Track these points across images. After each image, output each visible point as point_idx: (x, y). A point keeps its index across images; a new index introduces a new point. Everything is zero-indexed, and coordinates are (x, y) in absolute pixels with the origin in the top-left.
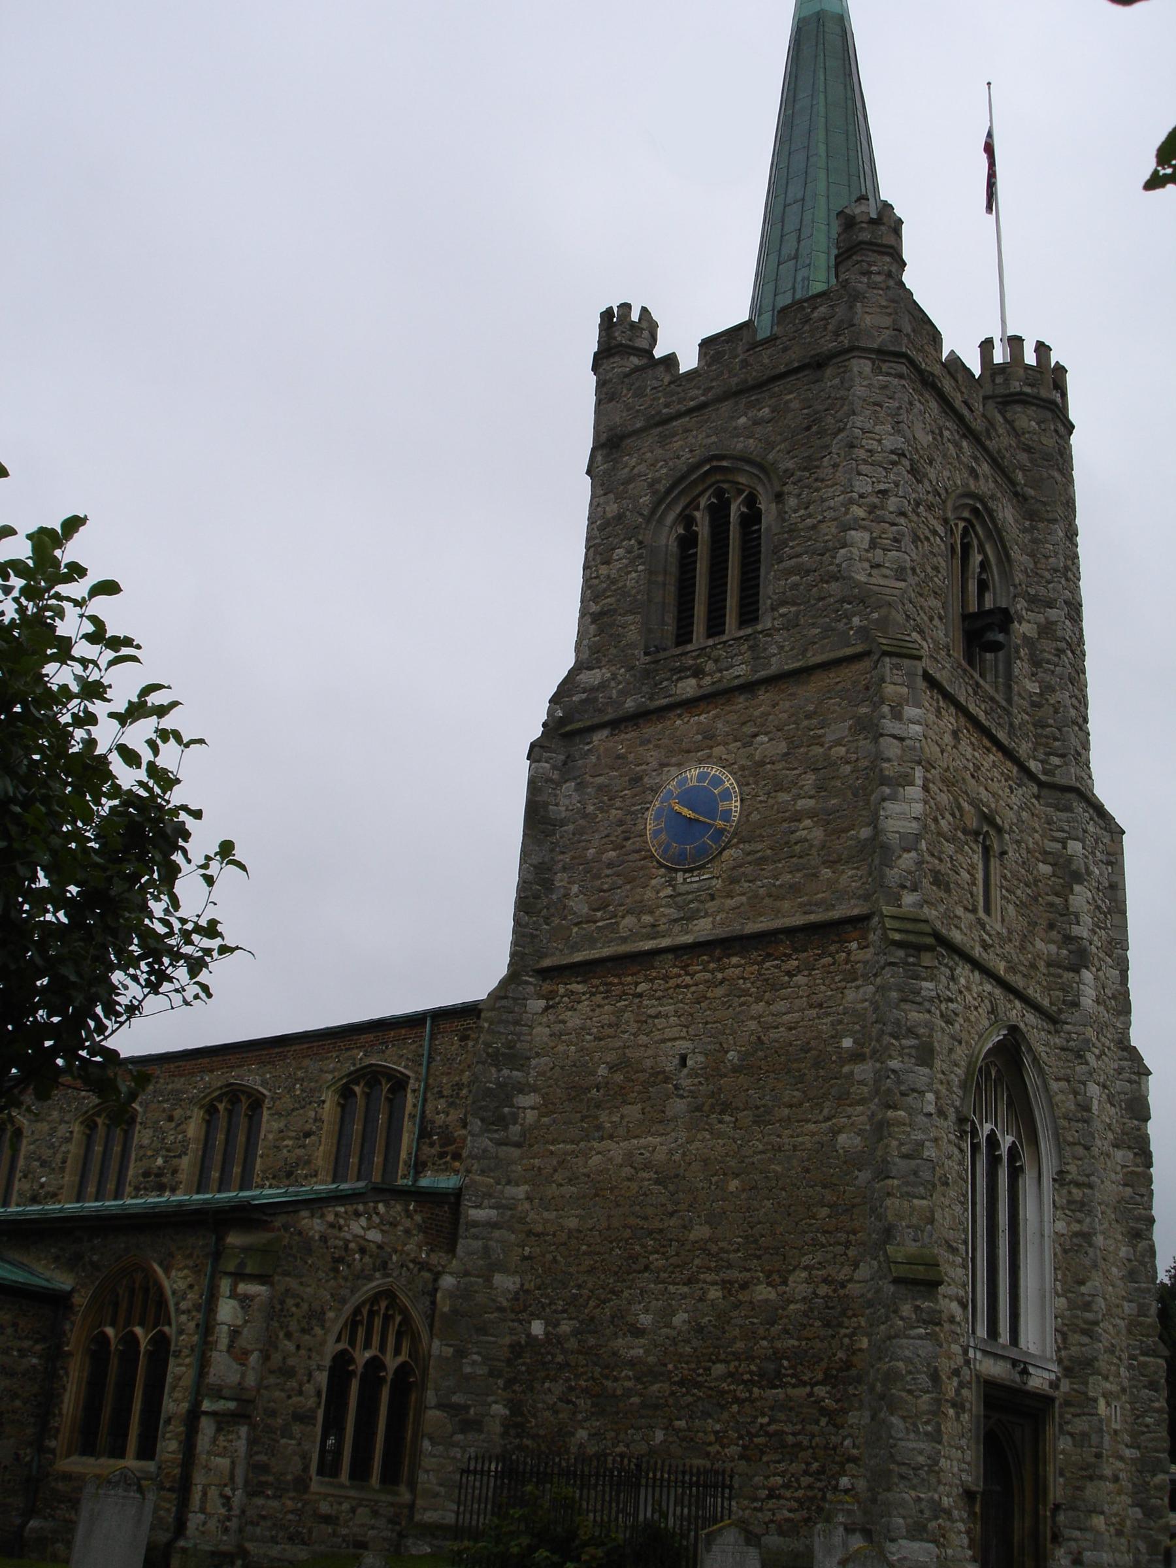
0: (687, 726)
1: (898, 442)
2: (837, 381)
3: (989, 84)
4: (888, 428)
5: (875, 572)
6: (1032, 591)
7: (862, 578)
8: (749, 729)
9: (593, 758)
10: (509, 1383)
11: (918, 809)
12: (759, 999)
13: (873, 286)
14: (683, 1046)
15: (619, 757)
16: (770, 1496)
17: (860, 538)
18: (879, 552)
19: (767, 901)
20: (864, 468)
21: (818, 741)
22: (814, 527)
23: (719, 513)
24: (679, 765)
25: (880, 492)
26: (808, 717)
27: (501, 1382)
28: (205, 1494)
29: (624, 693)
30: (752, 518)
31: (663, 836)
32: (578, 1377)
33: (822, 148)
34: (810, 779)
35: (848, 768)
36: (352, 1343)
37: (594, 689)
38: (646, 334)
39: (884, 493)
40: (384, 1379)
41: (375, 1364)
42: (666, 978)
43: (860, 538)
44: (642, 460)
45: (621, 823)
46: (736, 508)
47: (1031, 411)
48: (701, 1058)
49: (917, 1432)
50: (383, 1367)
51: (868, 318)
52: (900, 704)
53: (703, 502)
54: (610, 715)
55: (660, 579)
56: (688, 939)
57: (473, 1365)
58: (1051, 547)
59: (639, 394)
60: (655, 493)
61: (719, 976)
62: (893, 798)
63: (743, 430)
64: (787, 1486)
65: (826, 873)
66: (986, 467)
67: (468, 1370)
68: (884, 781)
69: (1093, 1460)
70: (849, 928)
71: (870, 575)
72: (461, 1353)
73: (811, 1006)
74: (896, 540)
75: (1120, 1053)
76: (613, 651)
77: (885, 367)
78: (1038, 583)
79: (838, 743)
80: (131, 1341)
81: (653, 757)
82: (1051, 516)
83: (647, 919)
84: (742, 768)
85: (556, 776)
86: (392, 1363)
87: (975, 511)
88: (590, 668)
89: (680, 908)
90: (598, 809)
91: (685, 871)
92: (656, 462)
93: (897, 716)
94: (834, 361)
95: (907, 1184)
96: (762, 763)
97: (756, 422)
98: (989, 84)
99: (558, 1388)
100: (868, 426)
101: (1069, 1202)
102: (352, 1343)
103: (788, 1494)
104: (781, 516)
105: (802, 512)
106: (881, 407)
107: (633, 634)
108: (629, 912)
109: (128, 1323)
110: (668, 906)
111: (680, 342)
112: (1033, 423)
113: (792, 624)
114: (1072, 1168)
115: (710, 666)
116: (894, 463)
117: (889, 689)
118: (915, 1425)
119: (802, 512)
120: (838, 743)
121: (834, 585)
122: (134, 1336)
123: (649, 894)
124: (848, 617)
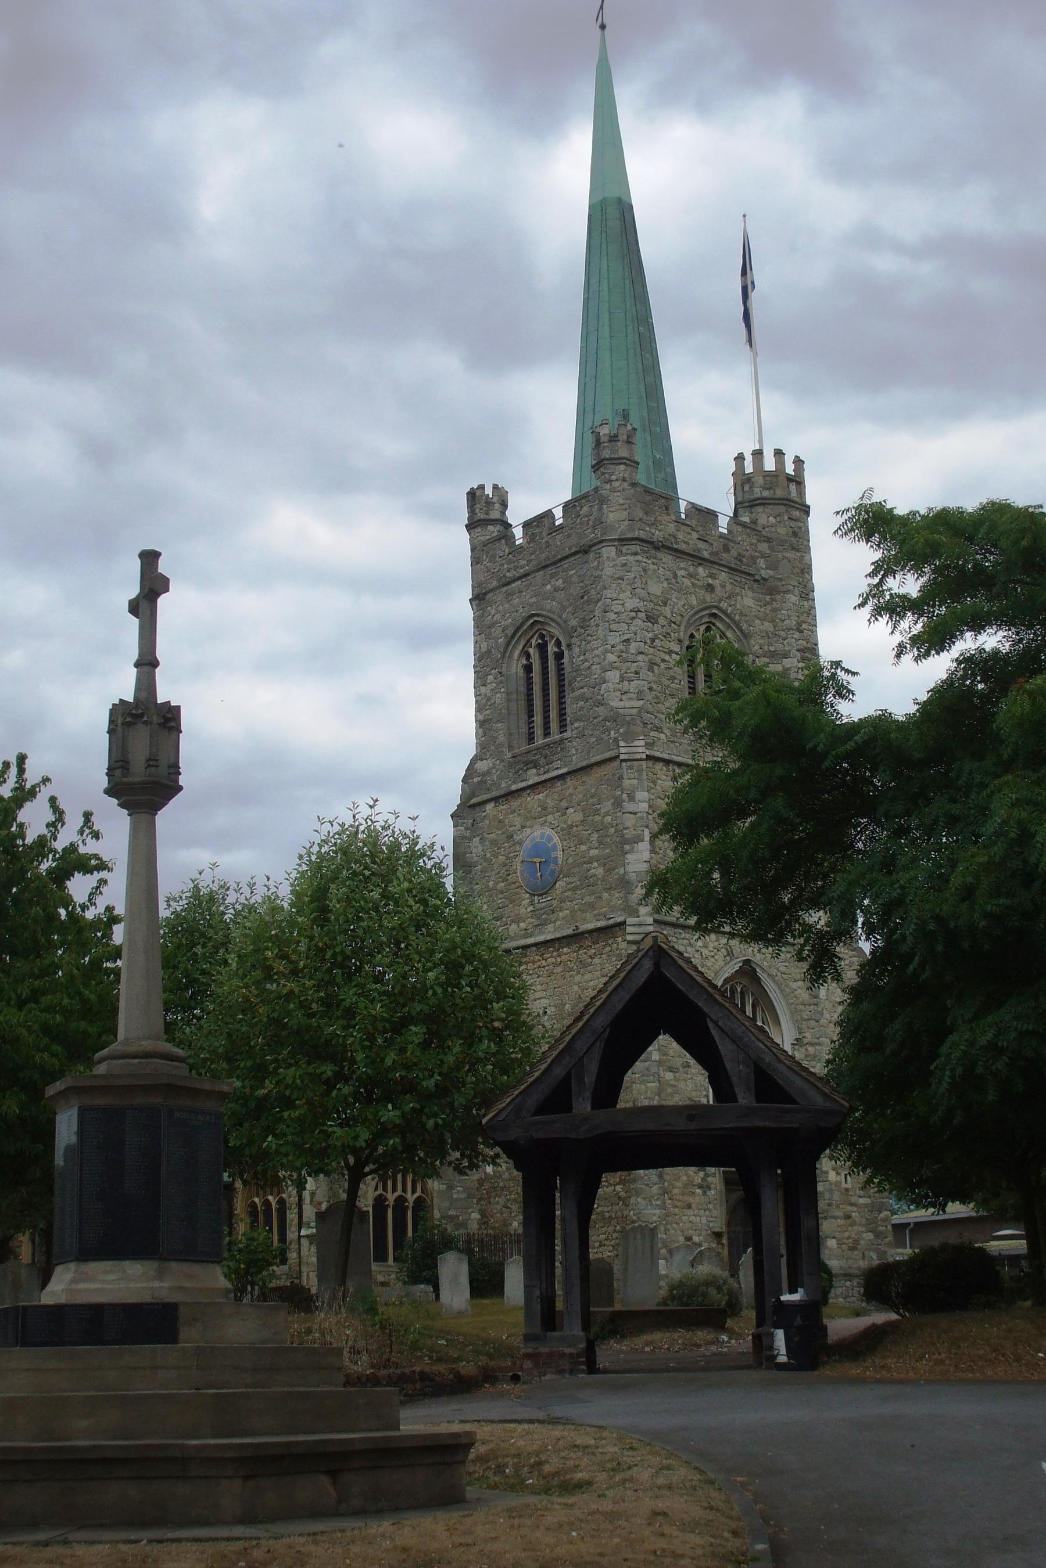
0: (533, 801)
1: (632, 603)
2: (595, 564)
3: (744, 216)
4: (628, 593)
5: (624, 697)
6: (772, 649)
7: (615, 704)
8: (564, 804)
9: (487, 822)
10: (480, 1200)
11: (646, 856)
12: (578, 973)
13: (613, 490)
14: (545, 1002)
15: (500, 822)
16: (600, 1246)
17: (613, 676)
18: (626, 683)
19: (579, 913)
20: (614, 627)
21: (597, 812)
22: (589, 668)
23: (542, 648)
24: (531, 827)
25: (624, 641)
26: (592, 797)
27: (475, 1201)
28: (308, 1275)
29: (500, 778)
30: (559, 656)
31: (525, 874)
32: (510, 1193)
33: (607, 328)
34: (595, 836)
35: (613, 830)
36: (385, 1189)
37: (484, 774)
38: (497, 506)
39: (627, 641)
40: (388, 1206)
41: (401, 1201)
42: (534, 962)
43: (613, 676)
44: (498, 612)
45: (505, 865)
46: (551, 649)
47: (769, 509)
48: (553, 1009)
49: (651, 1204)
50: (406, 1200)
51: (611, 515)
52: (633, 791)
53: (533, 641)
54: (495, 793)
55: (514, 696)
56: (541, 938)
57: (458, 1193)
58: (785, 612)
59: (492, 559)
60: (506, 636)
61: (559, 960)
62: (631, 851)
63: (547, 596)
64: (606, 1239)
65: (605, 895)
66: (723, 576)
67: (455, 1196)
68: (627, 842)
69: (826, 1207)
70: (617, 929)
71: (621, 700)
72: (450, 1187)
73: (603, 976)
74: (637, 673)
75: (851, 953)
76: (492, 748)
77: (624, 549)
78: (777, 641)
79: (607, 814)
80: (267, 1203)
81: (518, 821)
82: (784, 589)
83: (523, 925)
84: (562, 829)
85: (468, 834)
86: (411, 1198)
87: (714, 615)
88: (482, 760)
89: (538, 919)
90: (493, 855)
91: (539, 895)
92: (508, 612)
93: (631, 798)
94: (594, 548)
95: (643, 1075)
96: (571, 827)
97: (556, 589)
98: (744, 216)
99: (502, 1200)
100: (614, 596)
101: (806, 1056)
102: (385, 1189)
103: (608, 1243)
104: (571, 657)
105: (582, 658)
106: (623, 579)
107: (502, 738)
108: (513, 921)
109: (265, 1195)
110: (532, 917)
111: (520, 511)
112: (771, 518)
113: (581, 735)
114: (808, 1035)
115: (542, 761)
116: (633, 619)
117: (626, 783)
118: (650, 1201)
119: (582, 658)
120: (607, 814)
121: (601, 709)
122: (268, 1201)
123: (522, 910)
124: (608, 730)
